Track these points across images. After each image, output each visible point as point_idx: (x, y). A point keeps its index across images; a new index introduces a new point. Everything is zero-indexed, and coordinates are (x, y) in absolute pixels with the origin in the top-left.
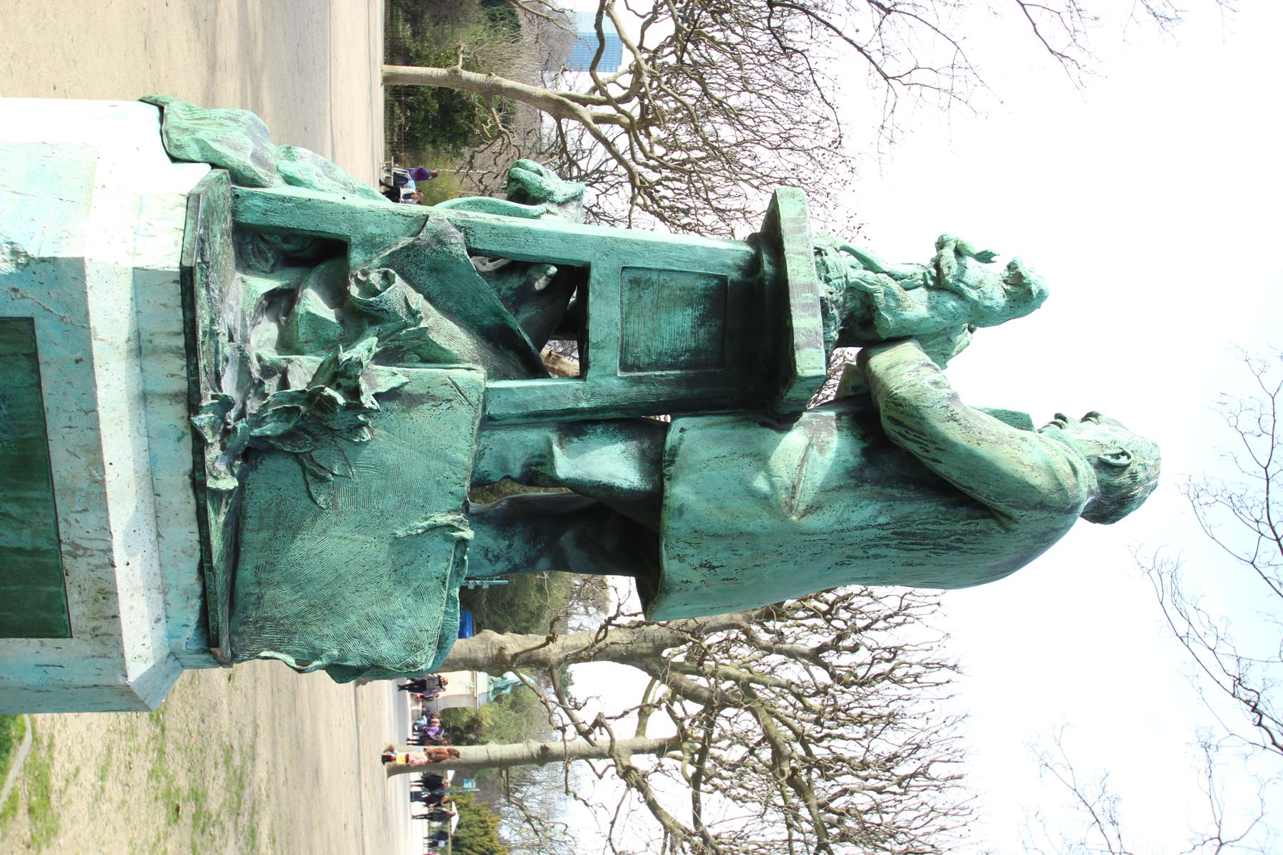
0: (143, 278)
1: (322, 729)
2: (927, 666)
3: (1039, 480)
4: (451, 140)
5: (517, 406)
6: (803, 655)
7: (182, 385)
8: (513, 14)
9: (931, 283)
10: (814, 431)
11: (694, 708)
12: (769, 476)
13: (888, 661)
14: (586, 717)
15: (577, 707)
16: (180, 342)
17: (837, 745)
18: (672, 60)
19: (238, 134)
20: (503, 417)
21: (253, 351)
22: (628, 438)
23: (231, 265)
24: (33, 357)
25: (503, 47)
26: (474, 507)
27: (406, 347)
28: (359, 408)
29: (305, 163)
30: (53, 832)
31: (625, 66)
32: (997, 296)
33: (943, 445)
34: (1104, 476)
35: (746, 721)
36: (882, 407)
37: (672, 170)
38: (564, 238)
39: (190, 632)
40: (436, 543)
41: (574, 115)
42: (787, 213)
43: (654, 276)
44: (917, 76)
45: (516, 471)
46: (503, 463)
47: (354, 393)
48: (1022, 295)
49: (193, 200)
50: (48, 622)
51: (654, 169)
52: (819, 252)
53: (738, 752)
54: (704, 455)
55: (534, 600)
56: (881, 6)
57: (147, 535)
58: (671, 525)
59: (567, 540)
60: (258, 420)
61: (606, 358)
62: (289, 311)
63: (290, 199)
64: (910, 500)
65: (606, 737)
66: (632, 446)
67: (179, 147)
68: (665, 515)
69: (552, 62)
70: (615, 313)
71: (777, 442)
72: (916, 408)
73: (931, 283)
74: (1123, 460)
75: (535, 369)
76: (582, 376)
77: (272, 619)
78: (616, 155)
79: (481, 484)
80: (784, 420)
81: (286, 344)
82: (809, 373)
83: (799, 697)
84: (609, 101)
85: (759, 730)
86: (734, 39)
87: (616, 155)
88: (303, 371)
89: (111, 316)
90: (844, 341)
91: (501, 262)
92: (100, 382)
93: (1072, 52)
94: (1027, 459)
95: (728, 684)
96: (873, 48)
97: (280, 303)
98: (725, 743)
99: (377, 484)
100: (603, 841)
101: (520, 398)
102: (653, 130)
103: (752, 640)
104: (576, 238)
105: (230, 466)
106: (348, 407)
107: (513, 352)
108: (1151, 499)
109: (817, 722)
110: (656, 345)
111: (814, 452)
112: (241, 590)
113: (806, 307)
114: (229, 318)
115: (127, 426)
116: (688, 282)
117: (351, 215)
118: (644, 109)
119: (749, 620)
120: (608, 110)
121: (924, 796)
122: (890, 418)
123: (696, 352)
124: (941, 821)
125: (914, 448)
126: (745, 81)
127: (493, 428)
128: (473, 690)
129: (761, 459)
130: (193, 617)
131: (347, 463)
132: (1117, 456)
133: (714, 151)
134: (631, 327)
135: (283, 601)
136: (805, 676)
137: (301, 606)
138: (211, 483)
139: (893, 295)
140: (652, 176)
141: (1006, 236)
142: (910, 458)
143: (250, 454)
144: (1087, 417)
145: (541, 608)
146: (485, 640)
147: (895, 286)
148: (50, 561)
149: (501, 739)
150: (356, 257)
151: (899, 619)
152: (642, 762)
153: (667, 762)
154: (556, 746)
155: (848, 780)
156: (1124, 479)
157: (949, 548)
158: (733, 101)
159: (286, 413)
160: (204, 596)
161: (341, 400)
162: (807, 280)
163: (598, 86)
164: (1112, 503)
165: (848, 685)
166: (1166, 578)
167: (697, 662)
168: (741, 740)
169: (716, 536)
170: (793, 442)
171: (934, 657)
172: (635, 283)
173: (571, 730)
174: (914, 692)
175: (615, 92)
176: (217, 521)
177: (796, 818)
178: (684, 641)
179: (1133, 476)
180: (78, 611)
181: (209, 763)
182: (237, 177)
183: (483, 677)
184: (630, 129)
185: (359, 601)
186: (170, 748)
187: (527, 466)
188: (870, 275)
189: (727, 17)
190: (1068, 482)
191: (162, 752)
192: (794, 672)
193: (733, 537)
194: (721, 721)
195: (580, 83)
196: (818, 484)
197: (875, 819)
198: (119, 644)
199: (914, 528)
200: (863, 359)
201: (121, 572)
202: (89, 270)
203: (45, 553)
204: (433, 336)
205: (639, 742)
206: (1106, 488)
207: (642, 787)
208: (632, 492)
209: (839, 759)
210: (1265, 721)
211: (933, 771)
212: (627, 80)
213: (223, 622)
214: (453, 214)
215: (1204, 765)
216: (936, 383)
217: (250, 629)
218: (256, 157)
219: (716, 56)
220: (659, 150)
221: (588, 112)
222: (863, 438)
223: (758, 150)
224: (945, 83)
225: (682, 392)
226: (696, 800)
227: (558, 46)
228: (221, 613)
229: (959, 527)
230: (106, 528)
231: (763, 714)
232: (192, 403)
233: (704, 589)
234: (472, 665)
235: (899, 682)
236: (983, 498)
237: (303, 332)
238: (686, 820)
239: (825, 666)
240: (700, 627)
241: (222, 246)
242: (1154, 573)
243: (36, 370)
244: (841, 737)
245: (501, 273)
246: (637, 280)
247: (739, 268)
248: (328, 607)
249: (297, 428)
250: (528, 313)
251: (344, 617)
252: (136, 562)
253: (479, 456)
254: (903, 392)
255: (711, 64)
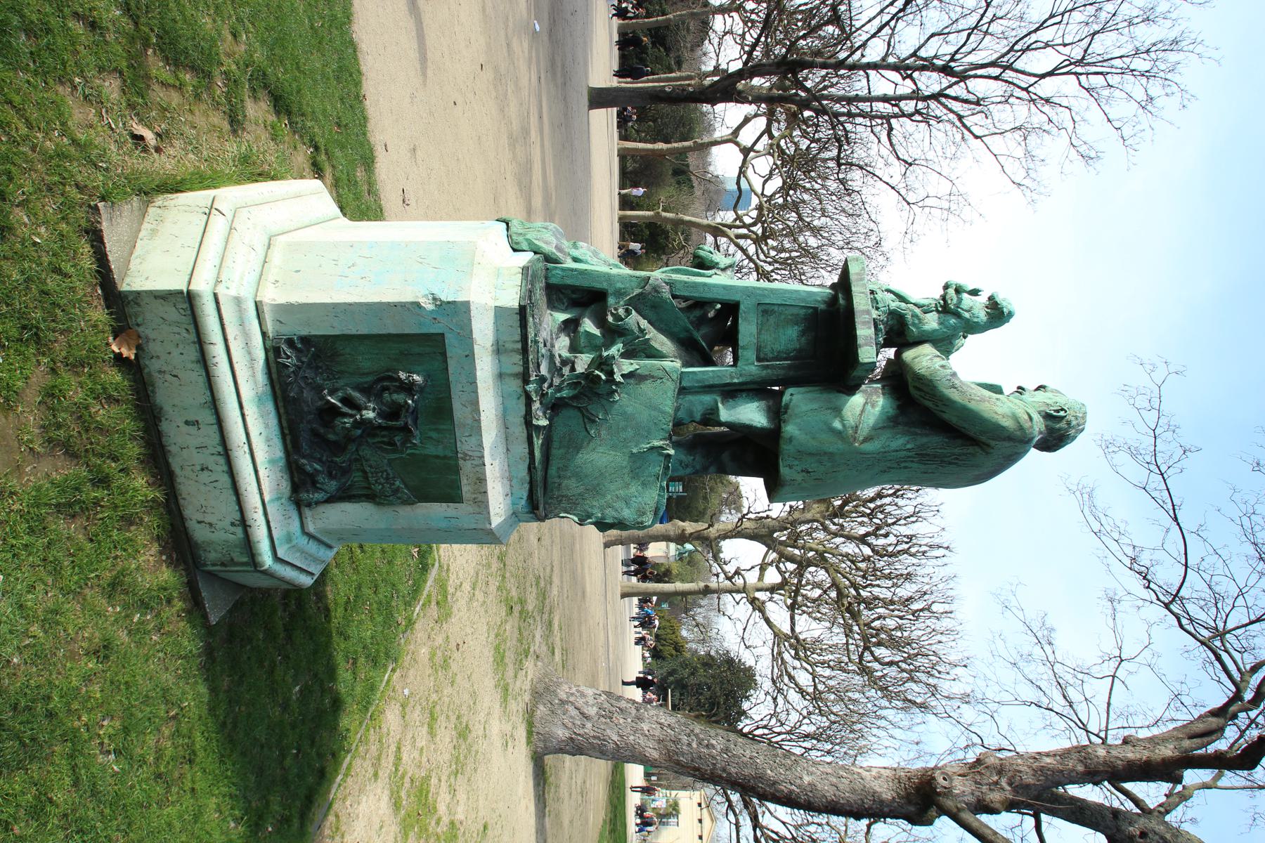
0: (500, 312)
1: (586, 570)
2: (930, 546)
3: (1007, 423)
4: (655, 252)
5: (698, 381)
6: (856, 538)
7: (520, 369)
8: (690, 180)
10: (868, 395)
11: (791, 566)
12: (842, 420)
14: (731, 569)
15: (725, 563)
16: (519, 346)
17: (876, 591)
18: (780, 201)
19: (548, 236)
20: (691, 388)
21: (556, 352)
22: (760, 399)
23: (545, 306)
24: (444, 354)
25: (684, 198)
26: (674, 438)
27: (638, 349)
28: (613, 381)
29: (583, 251)
30: (448, 615)
31: (753, 206)
32: (982, 316)
33: (948, 403)
34: (1049, 423)
35: (822, 575)
36: (910, 380)
37: (781, 264)
38: (725, 287)
39: (523, 502)
40: (654, 456)
41: (724, 235)
42: (853, 269)
43: (776, 308)
44: (928, 202)
45: (698, 417)
46: (690, 413)
47: (610, 373)
48: (997, 315)
49: (525, 270)
50: (451, 495)
51: (770, 263)
52: (872, 292)
53: (817, 593)
54: (804, 408)
55: (701, 505)
56: (906, 162)
57: (502, 449)
58: (785, 448)
59: (726, 457)
60: (559, 389)
61: (748, 354)
62: (575, 330)
63: (576, 270)
64: (927, 435)
65: (741, 581)
66: (763, 404)
67: (517, 243)
68: (781, 442)
69: (712, 206)
70: (754, 329)
71: (846, 402)
74: (1062, 413)
75: (709, 362)
76: (735, 365)
77: (566, 496)
78: (748, 257)
79: (678, 424)
80: (852, 390)
81: (574, 348)
82: (866, 361)
83: (853, 562)
84: (744, 226)
85: (829, 580)
86: (817, 186)
87: (748, 257)
88: (583, 362)
89: (483, 332)
90: (887, 344)
91: (689, 302)
92: (478, 368)
93: (1027, 182)
94: (1000, 410)
95: (811, 554)
96: (901, 187)
97: (570, 327)
98: (809, 587)
99: (622, 424)
100: (739, 640)
101: (700, 377)
102: (770, 241)
103: (825, 529)
104: (731, 287)
105: (545, 413)
106: (607, 381)
107: (696, 352)
108: (1080, 437)
109: (864, 577)
110: (777, 347)
111: (869, 407)
112: (550, 480)
114: (544, 335)
115: (491, 391)
116: (795, 311)
117: (608, 277)
118: (764, 230)
119: (824, 517)
120: (744, 231)
121: (928, 622)
122: (915, 387)
123: (799, 351)
124: (939, 637)
125: (929, 404)
126: (823, 210)
127: (686, 394)
128: (667, 553)
129: (838, 411)
130: (525, 495)
131: (606, 413)
132: (1058, 411)
133: (806, 251)
134: (762, 337)
135: (572, 486)
136: (857, 550)
137: (581, 489)
138: (535, 422)
139: (917, 316)
140: (769, 268)
141: (986, 279)
142: (927, 409)
143: (555, 407)
144: (1038, 389)
145: (705, 509)
146: (674, 525)
147: (918, 311)
148: (452, 462)
149: (683, 581)
150: (611, 300)
151: (914, 519)
152: (762, 596)
153: (776, 597)
154: (713, 584)
155: (881, 611)
156: (1063, 425)
157: (950, 463)
158: (816, 223)
159: (574, 385)
160: (531, 483)
161: (603, 377)
162: (865, 308)
163: (739, 218)
164: (1056, 433)
165: (882, 556)
166: (1086, 496)
167: (794, 539)
168: (817, 585)
169: (811, 454)
170: (857, 400)
171: (936, 541)
172: (765, 312)
173: (722, 576)
174: (923, 561)
175: (748, 220)
176: (538, 442)
177: (851, 631)
178: (786, 529)
179: (1069, 423)
180: (466, 489)
181: (528, 584)
182: (548, 259)
183: (673, 546)
184: (758, 241)
185: (613, 487)
186: (508, 575)
187: (704, 415)
188: (903, 305)
189: (813, 174)
190: (1027, 425)
191: (504, 577)
192: (850, 548)
193: (820, 455)
194: (807, 575)
195: (729, 217)
197: (899, 634)
198: (487, 507)
199: (929, 451)
200: (898, 354)
201: (488, 468)
202: (473, 307)
203: (450, 458)
204: (653, 343)
205: (760, 585)
206: (1050, 430)
207: (762, 611)
208: (762, 429)
209: (876, 598)
210: (1152, 585)
211: (934, 608)
212: (754, 214)
213: (541, 498)
214: (663, 276)
215: (1110, 611)
216: (943, 366)
217: (555, 501)
218: (558, 248)
219: (806, 197)
220: (773, 253)
221: (732, 232)
222: (898, 399)
223: (831, 250)
224: (946, 205)
225: (791, 373)
226: (792, 618)
227: (715, 197)
228: (540, 492)
229: (957, 451)
230: (481, 445)
231: (831, 571)
232: (526, 381)
233: (804, 485)
234: (666, 538)
235: (913, 555)
236: (972, 434)
237: (583, 341)
238: (786, 628)
239: (869, 545)
240: (795, 521)
241: (540, 296)
242: (1078, 493)
243: (446, 361)
244: (878, 586)
245: (689, 308)
246: (768, 310)
247: (825, 302)
248: (596, 490)
249: (580, 393)
250: (705, 330)
251: (604, 496)
252: (496, 463)
253: (677, 409)
254: (923, 371)
255: (804, 201)
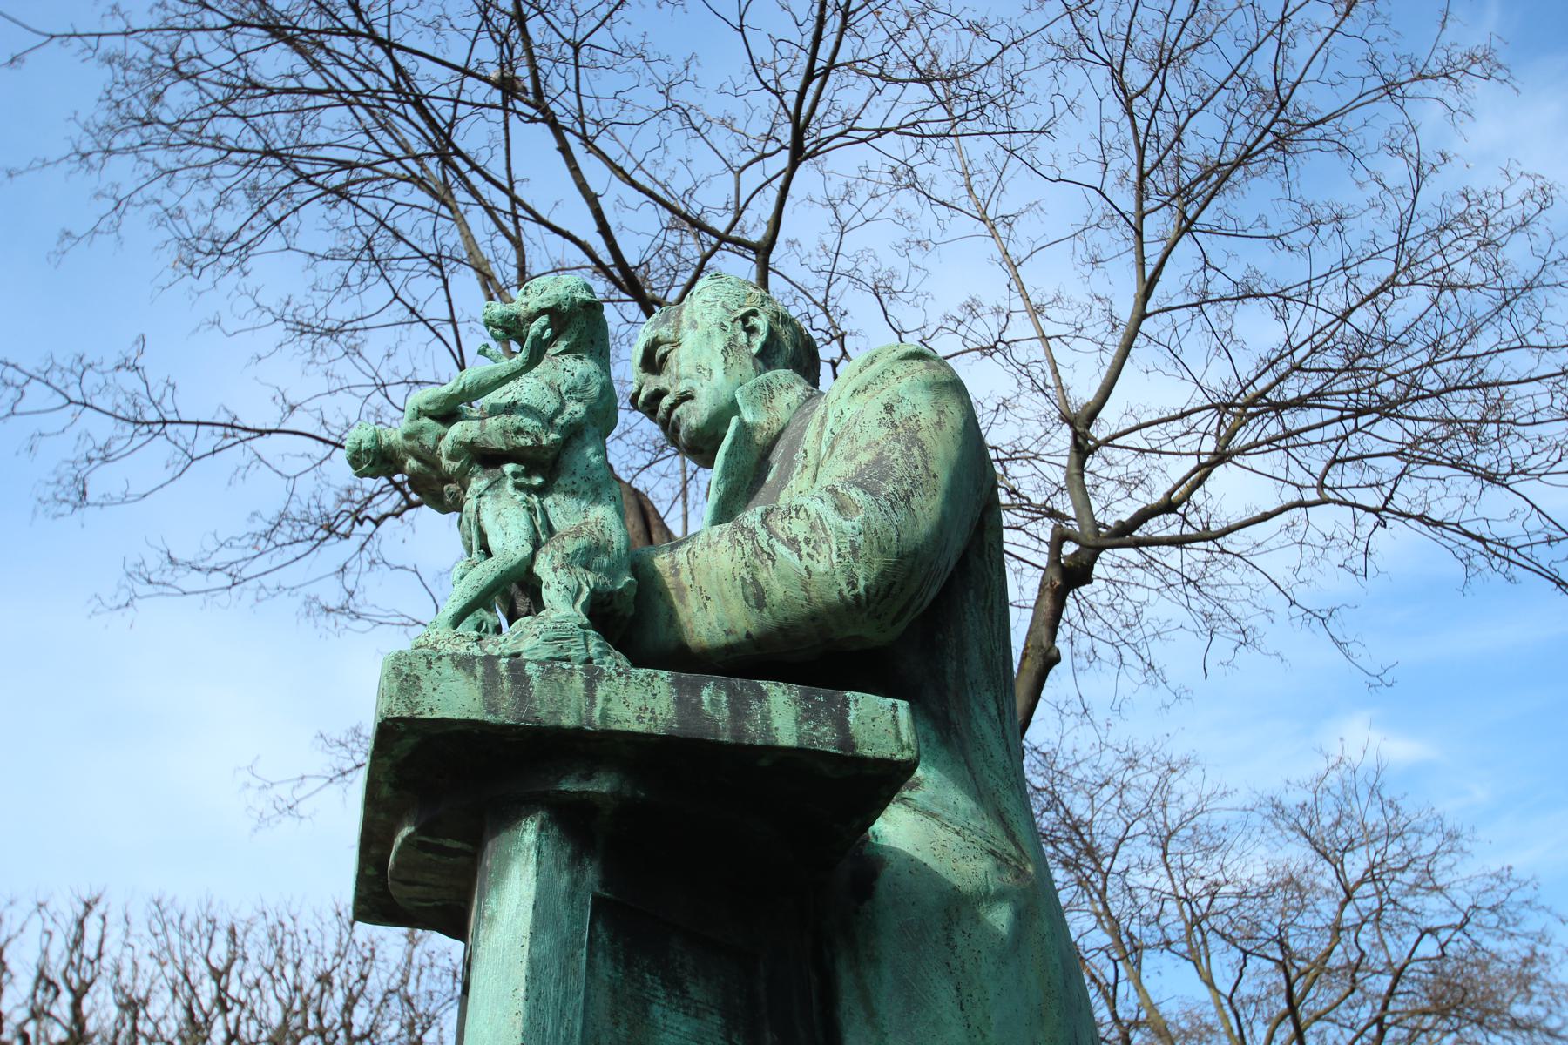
9: (537, 481)
13: (57, 993)
34: (779, 360)
72: (901, 556)
73: (537, 481)
113: (739, 711)
196: (973, 805)
247: (576, 861)
